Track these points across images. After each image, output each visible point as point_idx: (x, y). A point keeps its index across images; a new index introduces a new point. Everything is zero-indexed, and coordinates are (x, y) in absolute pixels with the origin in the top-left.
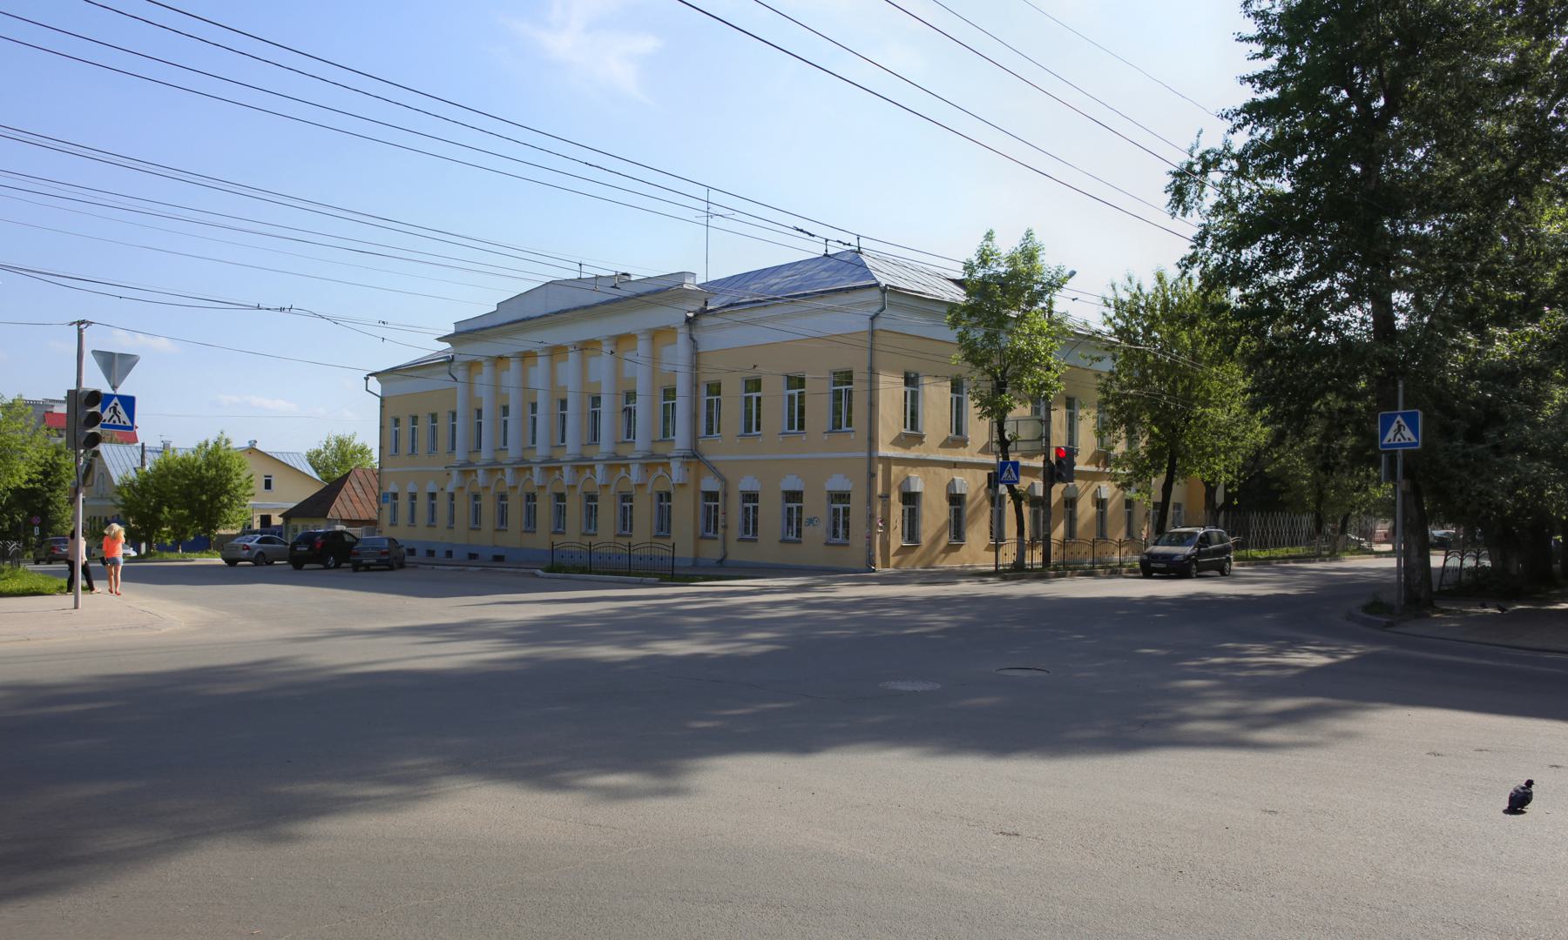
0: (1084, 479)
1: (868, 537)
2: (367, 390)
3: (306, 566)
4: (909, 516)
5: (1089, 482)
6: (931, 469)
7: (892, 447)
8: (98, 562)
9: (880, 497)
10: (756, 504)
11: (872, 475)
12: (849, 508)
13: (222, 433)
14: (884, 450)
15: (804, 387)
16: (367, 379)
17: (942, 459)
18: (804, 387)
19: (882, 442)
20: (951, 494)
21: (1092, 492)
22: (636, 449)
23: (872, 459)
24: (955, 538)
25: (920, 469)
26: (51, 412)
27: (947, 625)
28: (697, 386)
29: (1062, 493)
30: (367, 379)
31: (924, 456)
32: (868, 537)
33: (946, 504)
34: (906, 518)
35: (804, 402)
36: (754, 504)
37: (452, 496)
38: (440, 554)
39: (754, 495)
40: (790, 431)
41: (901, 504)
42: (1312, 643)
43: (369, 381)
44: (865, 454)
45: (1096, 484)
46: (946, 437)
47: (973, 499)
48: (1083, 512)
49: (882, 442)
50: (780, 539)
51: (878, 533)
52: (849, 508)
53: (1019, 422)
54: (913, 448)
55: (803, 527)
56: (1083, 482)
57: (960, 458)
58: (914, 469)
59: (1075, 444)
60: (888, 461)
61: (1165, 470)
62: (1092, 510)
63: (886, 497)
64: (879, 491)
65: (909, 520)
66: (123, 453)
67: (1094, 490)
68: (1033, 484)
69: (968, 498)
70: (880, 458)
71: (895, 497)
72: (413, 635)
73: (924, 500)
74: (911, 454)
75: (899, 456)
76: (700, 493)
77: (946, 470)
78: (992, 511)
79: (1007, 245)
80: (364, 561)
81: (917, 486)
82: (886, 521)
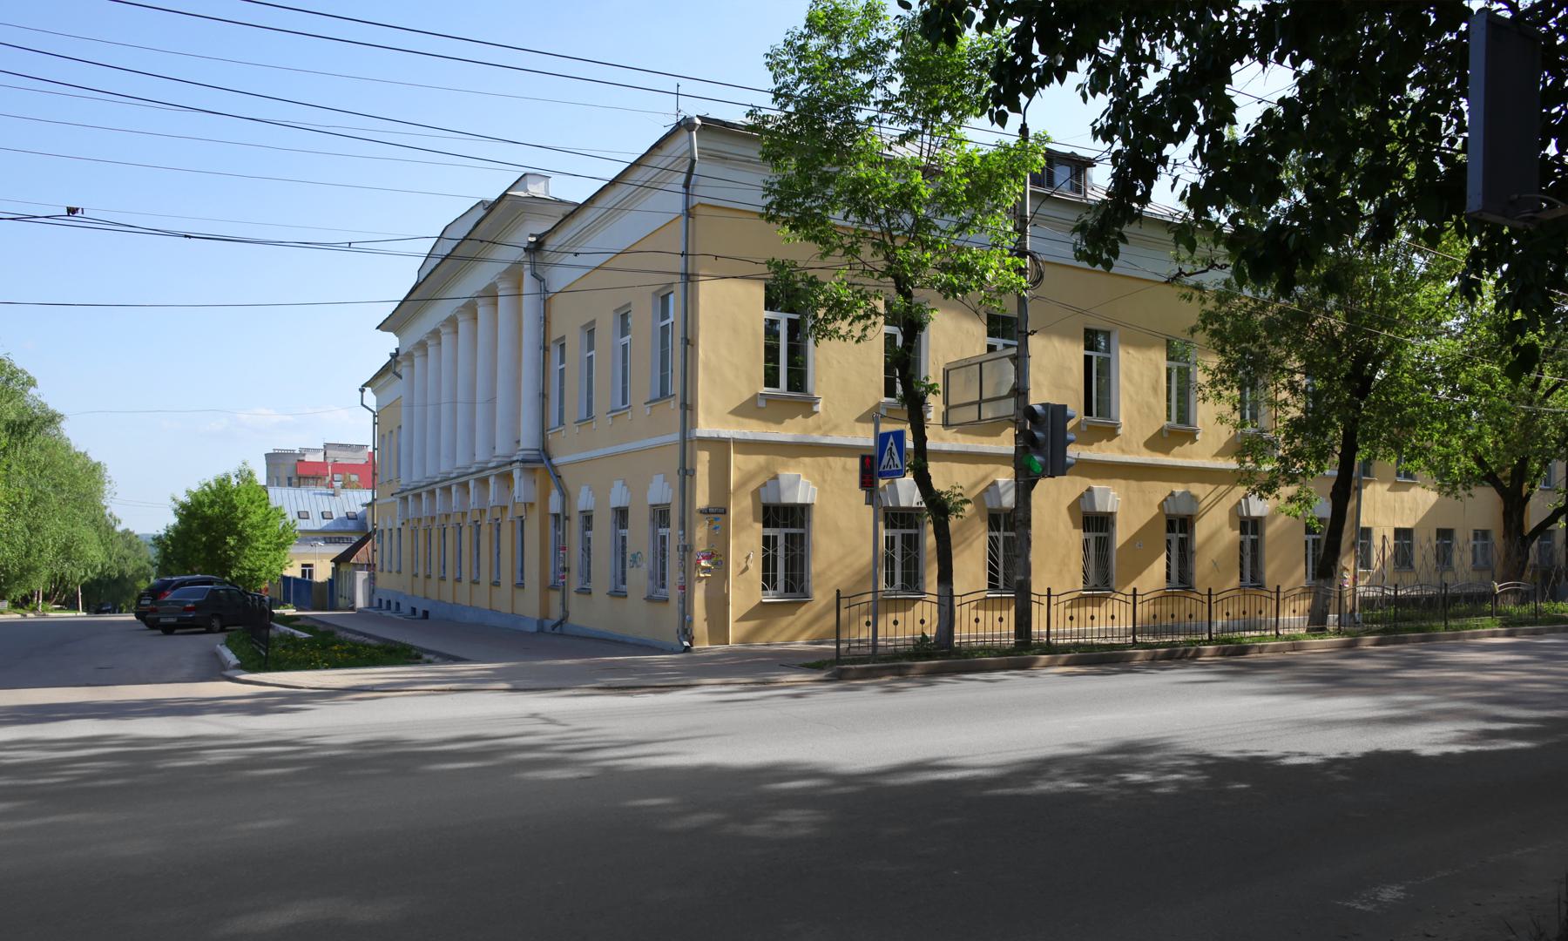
0: (1211, 483)
1: (683, 588)
2: (362, 404)
3: (177, 631)
4: (1314, 550)
5: (1223, 488)
7: (732, 418)
9: (702, 512)
11: (687, 472)
13: (244, 463)
14: (704, 428)
16: (362, 391)
19: (708, 411)
22: (496, 454)
23: (688, 443)
24: (903, 588)
25: (807, 460)
26: (303, 461)
28: (546, 349)
29: (1161, 506)
30: (362, 391)
31: (816, 437)
32: (683, 588)
33: (1078, 536)
34: (1310, 551)
35: (766, 369)
37: (400, 529)
38: (405, 609)
40: (625, 406)
41: (759, 526)
43: (365, 394)
44: (676, 437)
46: (871, 404)
48: (1210, 539)
49: (708, 411)
50: (645, 596)
51: (701, 579)
53: (983, 365)
54: (788, 422)
55: (628, 569)
56: (1209, 488)
58: (792, 462)
59: (1192, 422)
60: (720, 447)
61: (1337, 458)
62: (1231, 535)
63: (717, 512)
64: (702, 499)
65: (1313, 554)
66: (292, 497)
67: (1235, 501)
68: (1090, 490)
70: (702, 440)
71: (741, 507)
72: (807, 672)
73: (816, 519)
74: (787, 432)
75: (751, 437)
76: (550, 516)
78: (993, 543)
80: (162, 620)
82: (719, 558)
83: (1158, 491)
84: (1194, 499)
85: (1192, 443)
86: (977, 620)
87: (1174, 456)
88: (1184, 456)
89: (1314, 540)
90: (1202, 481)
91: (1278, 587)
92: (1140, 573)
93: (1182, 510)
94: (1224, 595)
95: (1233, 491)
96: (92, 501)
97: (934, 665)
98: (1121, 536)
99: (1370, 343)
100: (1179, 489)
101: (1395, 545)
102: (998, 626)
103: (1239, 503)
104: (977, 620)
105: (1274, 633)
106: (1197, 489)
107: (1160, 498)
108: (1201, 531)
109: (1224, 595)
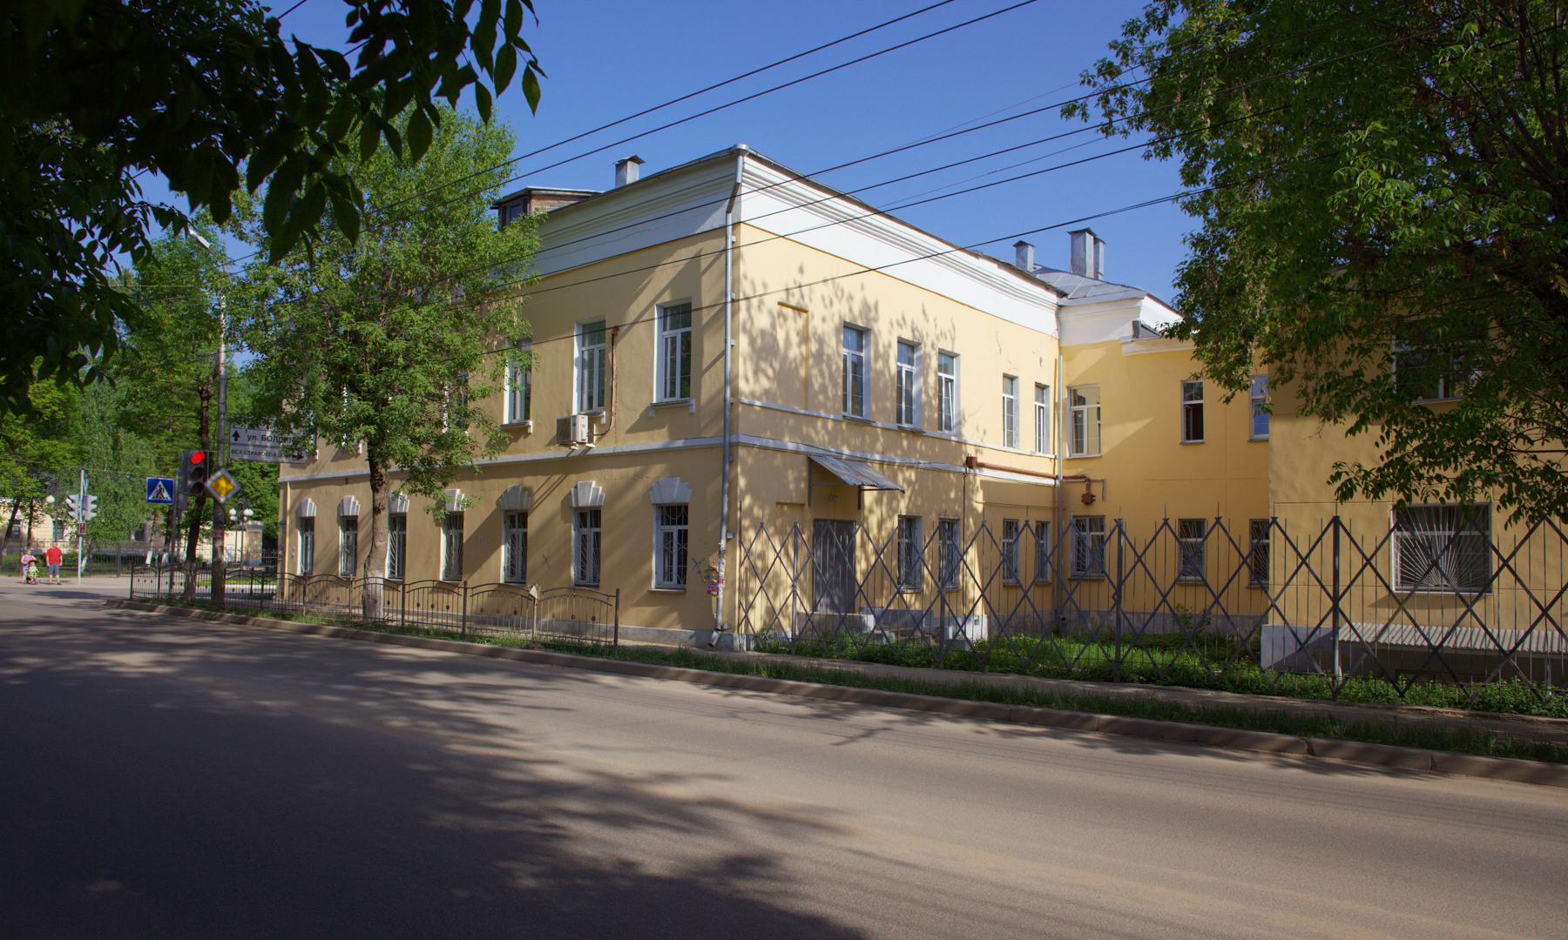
0: (543, 474)
5: (556, 477)
6: (323, 489)
8: (230, 603)
10: (597, 530)
12: (686, 531)
15: (689, 325)
17: (529, 459)
18: (689, 325)
20: (344, 517)
21: (561, 498)
27: (1287, 754)
36: (680, 527)
39: (680, 508)
42: (124, 642)
45: (573, 477)
47: (363, 519)
52: (686, 531)
56: (541, 479)
57: (349, 472)
69: (359, 520)
77: (338, 487)
79: (174, 193)
81: (311, 510)
83: (497, 488)
84: (528, 491)
85: (525, 437)
86: (418, 605)
87: (510, 453)
88: (519, 451)
89: (680, 531)
90: (535, 474)
91: (618, 590)
92: (480, 566)
93: (515, 505)
94: (417, 586)
95: (565, 481)
96: (420, 491)
97: (563, 658)
98: (468, 532)
99: (293, 397)
100: (510, 483)
101: (1268, 538)
102: (674, 633)
103: (570, 494)
104: (418, 605)
105: (406, 617)
106: (529, 481)
107: (497, 495)
108: (534, 522)
109: (417, 586)
